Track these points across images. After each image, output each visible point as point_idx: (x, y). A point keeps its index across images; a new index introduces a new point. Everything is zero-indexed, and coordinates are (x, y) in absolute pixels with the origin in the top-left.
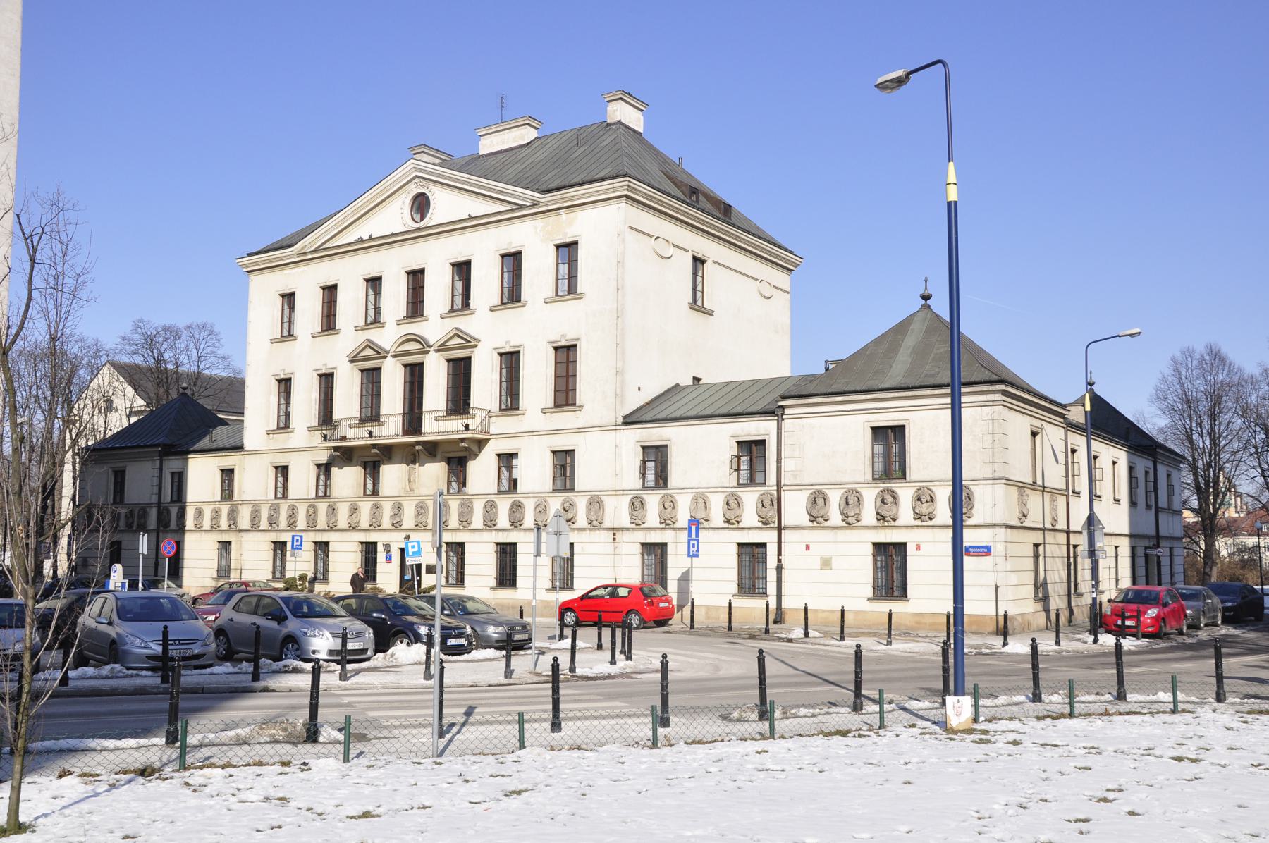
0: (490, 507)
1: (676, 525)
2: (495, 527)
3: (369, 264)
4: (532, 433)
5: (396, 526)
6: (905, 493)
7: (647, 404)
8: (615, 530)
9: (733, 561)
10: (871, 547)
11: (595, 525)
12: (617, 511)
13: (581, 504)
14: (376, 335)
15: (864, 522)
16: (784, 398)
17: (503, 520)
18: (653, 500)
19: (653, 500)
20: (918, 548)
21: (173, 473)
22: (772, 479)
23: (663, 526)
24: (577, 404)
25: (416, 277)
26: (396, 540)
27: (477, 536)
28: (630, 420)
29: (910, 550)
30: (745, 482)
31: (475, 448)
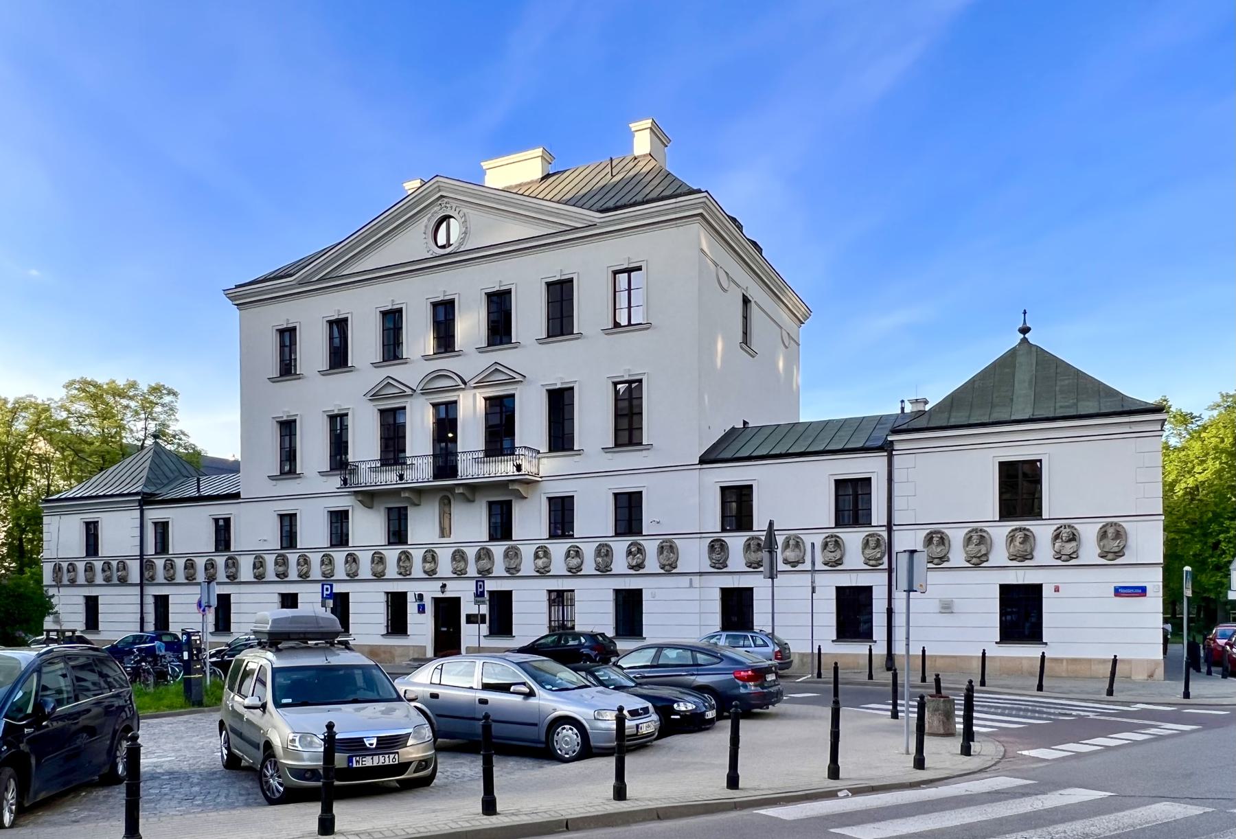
5: (431, 574)
6: (1042, 531)
11: (669, 568)
12: (693, 555)
13: (651, 547)
15: (78, 583)
17: (392, 570)
20: (1057, 590)
21: (156, 524)
24: (644, 442)
25: (339, 327)
26: (431, 590)
27: (243, 588)
28: (707, 459)
29: (1047, 592)
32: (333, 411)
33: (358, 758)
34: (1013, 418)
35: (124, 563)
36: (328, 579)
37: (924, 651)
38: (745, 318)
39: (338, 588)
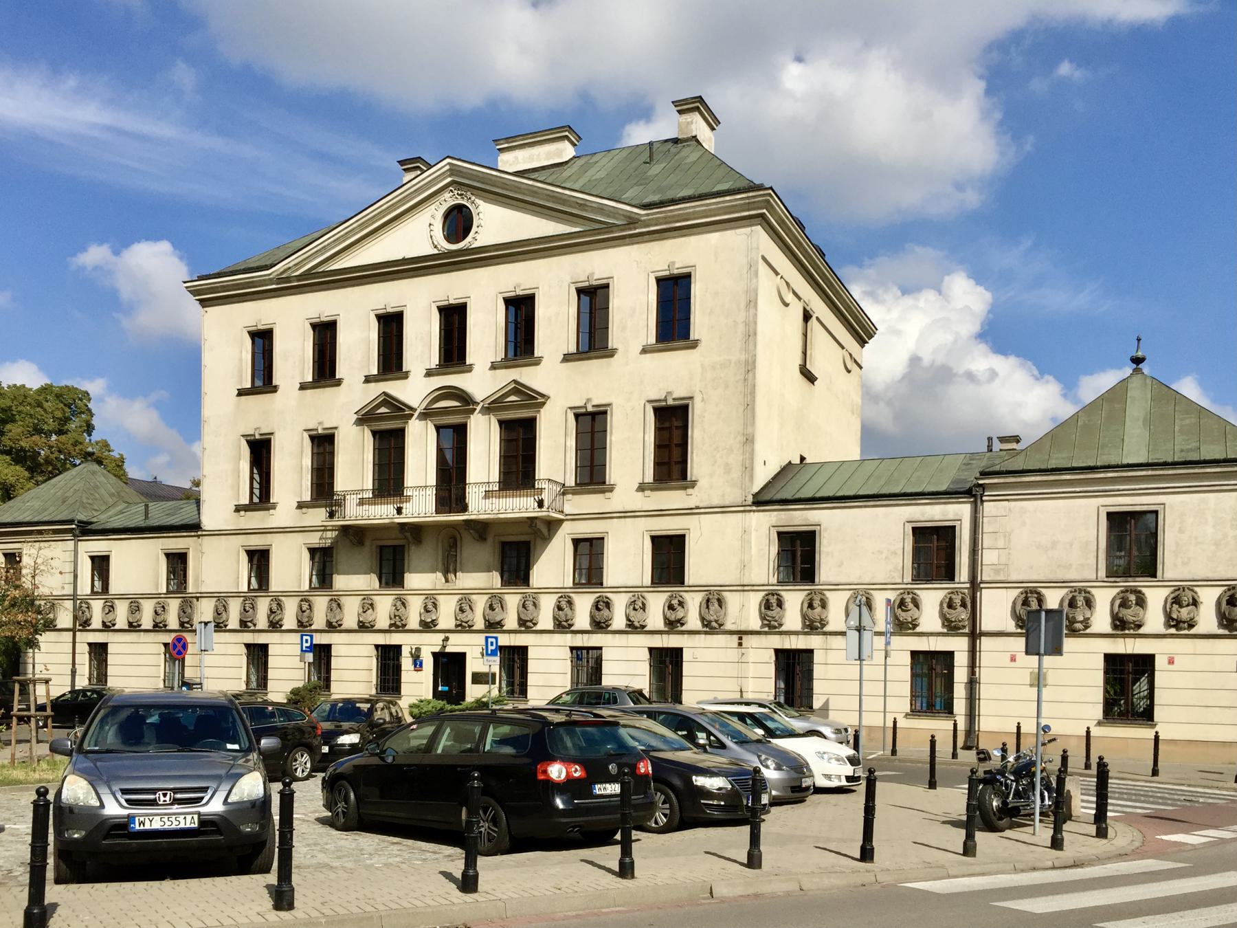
0: (565, 604)
1: (827, 629)
2: (572, 628)
3: (386, 296)
4: (625, 514)
5: (428, 626)
7: (769, 482)
8: (741, 634)
9: (1099, 678)
10: (773, 652)
11: (711, 627)
13: (694, 602)
14: (395, 388)
16: (984, 474)
18: (794, 599)
19: (794, 599)
20: (1171, 662)
22: (963, 573)
23: (766, 629)
28: (761, 501)
29: (1160, 663)
30: (657, 581)
31: (545, 530)
32: (317, 430)
33: (142, 819)
34: (1125, 461)
35: (1039, 593)
36: (303, 626)
37: (1019, 728)
38: (805, 335)
39: (320, 639)
